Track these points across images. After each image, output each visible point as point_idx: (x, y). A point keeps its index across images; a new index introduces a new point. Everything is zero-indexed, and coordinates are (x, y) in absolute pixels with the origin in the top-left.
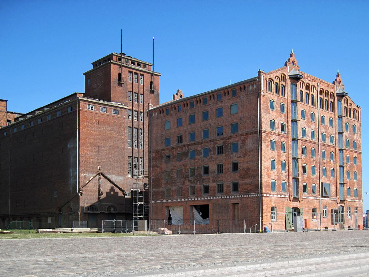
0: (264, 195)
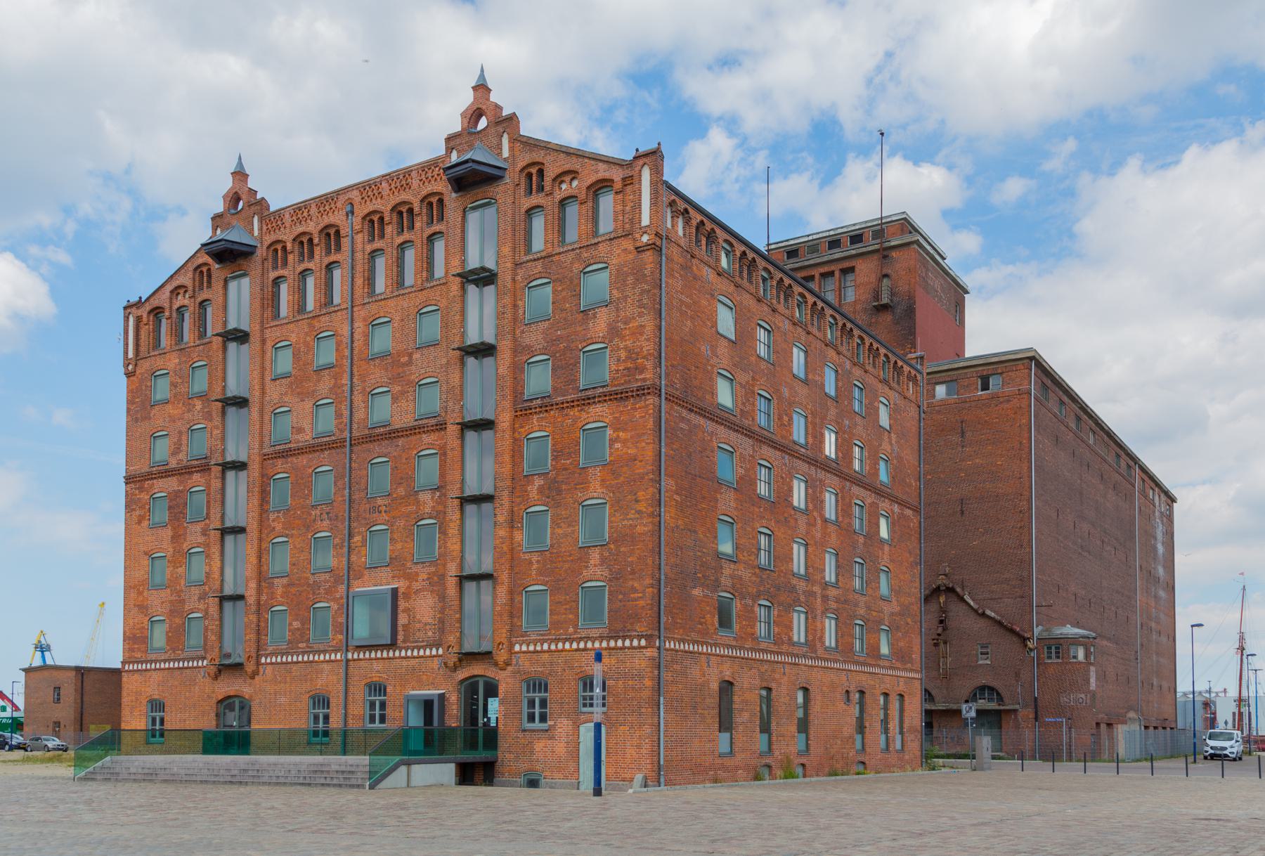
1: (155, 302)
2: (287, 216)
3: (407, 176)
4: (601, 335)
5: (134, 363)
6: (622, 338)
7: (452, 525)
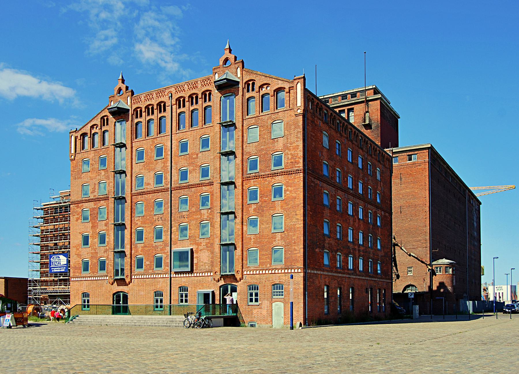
0: (72, 279)
1: (83, 131)
2: (143, 97)
3: (196, 83)
4: (280, 148)
5: (74, 155)
6: (289, 150)
7: (216, 223)
